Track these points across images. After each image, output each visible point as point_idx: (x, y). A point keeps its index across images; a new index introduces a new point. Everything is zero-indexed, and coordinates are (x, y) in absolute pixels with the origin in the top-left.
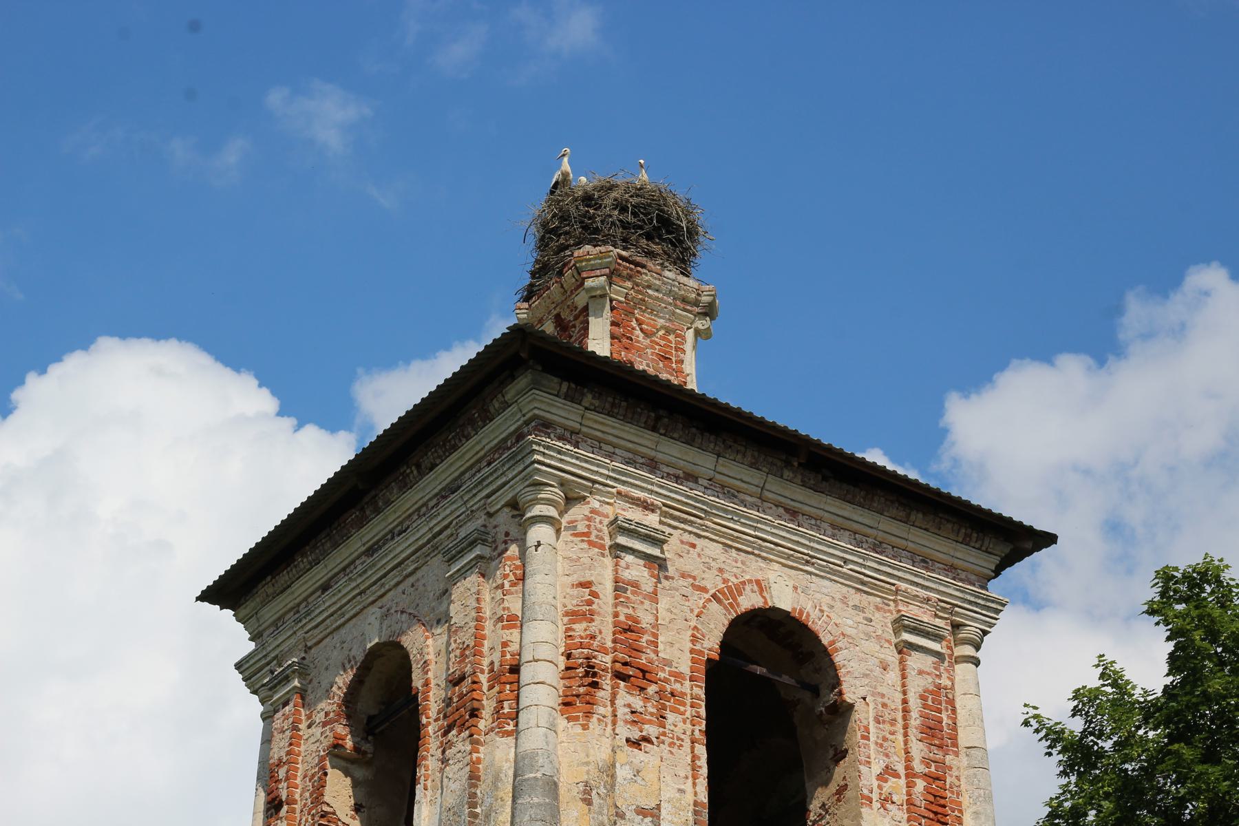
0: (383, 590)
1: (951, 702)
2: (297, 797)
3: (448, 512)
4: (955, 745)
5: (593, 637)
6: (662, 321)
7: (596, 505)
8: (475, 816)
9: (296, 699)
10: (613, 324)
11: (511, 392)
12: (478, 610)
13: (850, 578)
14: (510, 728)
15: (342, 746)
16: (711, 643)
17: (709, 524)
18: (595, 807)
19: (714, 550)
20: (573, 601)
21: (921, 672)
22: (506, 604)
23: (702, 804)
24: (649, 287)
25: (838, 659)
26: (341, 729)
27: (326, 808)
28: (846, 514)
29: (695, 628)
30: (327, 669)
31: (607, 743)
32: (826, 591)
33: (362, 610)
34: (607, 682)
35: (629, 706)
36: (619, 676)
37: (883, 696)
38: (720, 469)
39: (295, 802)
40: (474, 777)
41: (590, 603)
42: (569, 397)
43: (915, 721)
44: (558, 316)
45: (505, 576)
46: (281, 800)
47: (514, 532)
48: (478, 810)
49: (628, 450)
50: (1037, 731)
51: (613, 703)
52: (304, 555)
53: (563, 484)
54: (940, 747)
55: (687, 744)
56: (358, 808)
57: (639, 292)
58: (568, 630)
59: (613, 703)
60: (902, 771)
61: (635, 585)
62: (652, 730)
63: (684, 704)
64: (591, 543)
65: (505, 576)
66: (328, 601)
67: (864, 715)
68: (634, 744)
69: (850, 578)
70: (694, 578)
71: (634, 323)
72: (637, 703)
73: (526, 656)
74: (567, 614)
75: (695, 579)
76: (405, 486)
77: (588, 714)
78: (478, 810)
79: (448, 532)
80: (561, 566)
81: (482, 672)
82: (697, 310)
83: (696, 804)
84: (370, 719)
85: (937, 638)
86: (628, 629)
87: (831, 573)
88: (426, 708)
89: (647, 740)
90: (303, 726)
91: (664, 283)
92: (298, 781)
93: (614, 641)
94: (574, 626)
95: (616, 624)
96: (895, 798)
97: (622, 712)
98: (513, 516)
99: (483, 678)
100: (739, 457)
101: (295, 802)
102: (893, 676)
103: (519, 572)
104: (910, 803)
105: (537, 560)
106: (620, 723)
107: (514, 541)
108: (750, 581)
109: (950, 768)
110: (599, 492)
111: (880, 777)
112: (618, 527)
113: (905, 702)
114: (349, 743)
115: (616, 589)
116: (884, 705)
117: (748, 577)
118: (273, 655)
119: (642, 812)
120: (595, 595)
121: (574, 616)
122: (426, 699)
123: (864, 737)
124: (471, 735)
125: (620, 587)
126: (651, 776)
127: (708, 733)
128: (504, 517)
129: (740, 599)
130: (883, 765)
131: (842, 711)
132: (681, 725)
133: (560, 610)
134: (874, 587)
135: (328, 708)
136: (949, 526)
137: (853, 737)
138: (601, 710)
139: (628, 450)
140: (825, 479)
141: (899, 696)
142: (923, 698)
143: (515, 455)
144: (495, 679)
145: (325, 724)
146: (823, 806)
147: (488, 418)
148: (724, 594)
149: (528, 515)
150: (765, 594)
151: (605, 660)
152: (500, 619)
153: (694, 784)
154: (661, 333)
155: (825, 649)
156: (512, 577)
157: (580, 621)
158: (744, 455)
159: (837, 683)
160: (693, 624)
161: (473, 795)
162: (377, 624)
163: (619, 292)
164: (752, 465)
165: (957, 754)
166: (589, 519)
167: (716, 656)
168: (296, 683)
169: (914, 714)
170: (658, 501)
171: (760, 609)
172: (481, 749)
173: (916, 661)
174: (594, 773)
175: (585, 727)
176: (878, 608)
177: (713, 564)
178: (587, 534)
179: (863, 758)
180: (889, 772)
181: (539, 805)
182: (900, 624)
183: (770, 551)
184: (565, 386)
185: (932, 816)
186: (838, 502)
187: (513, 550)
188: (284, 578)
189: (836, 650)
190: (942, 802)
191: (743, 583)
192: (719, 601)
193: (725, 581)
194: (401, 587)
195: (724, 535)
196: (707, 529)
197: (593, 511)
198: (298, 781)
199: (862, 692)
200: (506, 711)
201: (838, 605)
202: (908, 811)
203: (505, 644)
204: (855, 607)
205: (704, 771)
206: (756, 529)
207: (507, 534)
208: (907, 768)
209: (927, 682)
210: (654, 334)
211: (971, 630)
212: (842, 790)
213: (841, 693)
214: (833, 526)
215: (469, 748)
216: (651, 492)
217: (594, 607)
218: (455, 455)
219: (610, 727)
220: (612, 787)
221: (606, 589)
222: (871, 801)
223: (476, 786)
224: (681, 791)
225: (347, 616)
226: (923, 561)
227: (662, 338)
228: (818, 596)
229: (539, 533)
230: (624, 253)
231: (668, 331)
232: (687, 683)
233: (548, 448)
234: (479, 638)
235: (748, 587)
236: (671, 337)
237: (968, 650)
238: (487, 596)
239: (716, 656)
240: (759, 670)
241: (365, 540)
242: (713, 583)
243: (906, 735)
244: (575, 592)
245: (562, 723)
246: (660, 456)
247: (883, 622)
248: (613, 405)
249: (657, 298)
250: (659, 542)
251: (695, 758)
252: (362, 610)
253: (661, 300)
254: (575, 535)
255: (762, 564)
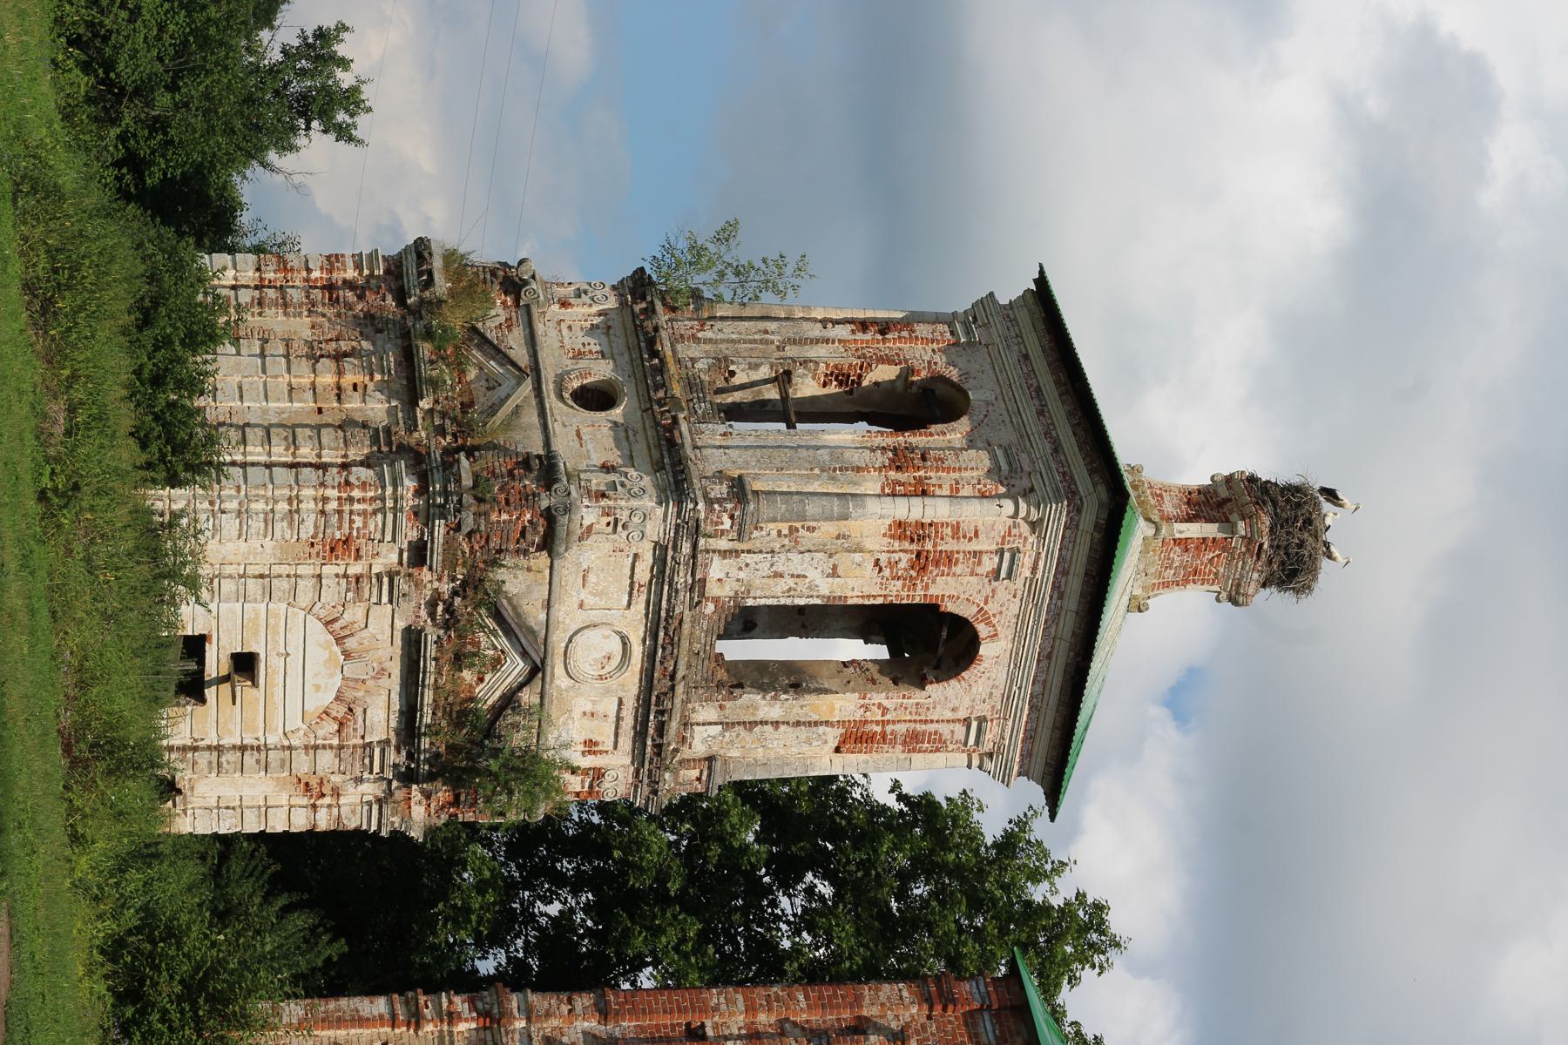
0: (1007, 399)
1: (937, 750)
2: (887, 345)
3: (1040, 446)
4: (909, 751)
5: (942, 539)
6: (1222, 570)
7: (1031, 540)
8: (835, 470)
9: (953, 340)
10: (1214, 539)
11: (1102, 489)
12: (966, 469)
13: (1010, 690)
14: (887, 491)
15: (913, 375)
16: (949, 607)
17: (1031, 606)
18: (836, 541)
19: (1014, 608)
20: (968, 528)
21: (952, 732)
22: (966, 487)
23: (846, 601)
24: (1244, 563)
25: (953, 682)
26: (924, 374)
27: (874, 366)
28: (1053, 689)
29: (958, 598)
30: (969, 361)
31: (877, 547)
32: (999, 675)
33: (1000, 385)
34: (914, 547)
35: (900, 560)
36: (918, 555)
37: (934, 708)
38: (1069, 613)
39: (884, 343)
40: (858, 469)
41: (964, 537)
42: (1097, 525)
43: (920, 727)
44: (1230, 500)
45: (985, 486)
46: (886, 334)
47: (1014, 490)
48: (838, 472)
49: (1071, 558)
50: (1025, 814)
51: (901, 551)
52: (1050, 342)
53: (1041, 520)
54: (905, 741)
55: (883, 593)
56: (876, 384)
57: (1239, 557)
58: (947, 524)
59: (901, 551)
60: (886, 718)
61: (979, 563)
62: (887, 572)
63: (909, 590)
64: (1004, 537)
65: (985, 486)
66: (1011, 358)
67: (918, 696)
68: (877, 563)
69: (1010, 690)
70: (993, 597)
71: (1217, 552)
72: (903, 565)
73: (927, 500)
74: (958, 523)
75: (993, 597)
76: (1070, 414)
77: (892, 537)
78: (838, 472)
79: (1028, 445)
80: (990, 520)
81: (926, 472)
82: (1233, 593)
83: (846, 597)
84: (933, 391)
85: (977, 743)
86: (950, 559)
87: (1011, 680)
88: (915, 435)
89: (881, 570)
90: (935, 346)
91: (1248, 573)
92: (898, 345)
93: (941, 551)
94: (950, 528)
95: (952, 552)
96: (868, 713)
97: (896, 556)
98: (1025, 490)
99: (922, 473)
100: (1077, 625)
101: (884, 343)
102: (949, 715)
103: (987, 494)
104: (866, 722)
105: (991, 506)
106: (888, 555)
107: (1008, 490)
108: (996, 630)
109: (893, 747)
110: (1039, 542)
111: (880, 705)
112: (1015, 553)
113: (932, 721)
114: (915, 378)
115: (975, 552)
116: (928, 709)
117: (999, 629)
118: (991, 320)
119: (835, 567)
120: (970, 539)
121: (956, 528)
122: (921, 435)
123: (904, 696)
124: (885, 467)
125: (976, 554)
126: (858, 572)
127: (891, 605)
128: (1026, 483)
129: (983, 624)
130: (889, 707)
131: (921, 683)
132: (895, 589)
133: (961, 520)
134: (1007, 706)
135: (939, 365)
136: (1055, 754)
137: (904, 690)
138: (897, 544)
139: (1071, 558)
140: (1073, 677)
141: (935, 718)
142: (936, 733)
143: (1058, 491)
144: (919, 481)
145: (929, 362)
146: (868, 670)
147: (1091, 472)
148: (984, 615)
149: (1020, 500)
150: (988, 639)
151: (929, 546)
152: (957, 483)
153: (858, 597)
154: (1214, 570)
155: (959, 674)
156: (984, 489)
157: (953, 531)
158: (1079, 628)
159: (938, 681)
160: (962, 596)
161: (847, 469)
162: (983, 398)
163: (1236, 542)
164: (1074, 632)
165: (903, 751)
166: (1020, 536)
167: (942, 609)
168: (963, 340)
169: (923, 727)
170: (1039, 576)
171: (978, 636)
172: (877, 473)
173: (960, 730)
174: (857, 541)
175: (884, 535)
176: (993, 707)
177: (1004, 608)
178: (1010, 535)
179: (890, 695)
180: (885, 711)
181: (832, 511)
182: (982, 720)
183: (1019, 642)
184: (1103, 522)
185: (859, 735)
186: (1059, 684)
187: (1002, 490)
188: (1041, 326)
189: (959, 681)
190: (869, 741)
191: (994, 626)
192: (979, 612)
193: (994, 615)
194: (1004, 412)
195: (1024, 615)
196: (1026, 606)
197: (1026, 539)
198: (898, 345)
199: (934, 695)
200: (897, 488)
201: (991, 683)
202: (860, 721)
203: (940, 486)
204: (991, 694)
205: (867, 602)
206: (1031, 634)
207: (1013, 486)
208: (888, 721)
209: (947, 736)
210: (1212, 565)
211: (989, 765)
212: (873, 682)
213: (931, 683)
214: (1045, 682)
215: (877, 466)
216: (1044, 572)
217: (962, 539)
218: (1077, 449)
219: (886, 549)
220: (849, 551)
221: (974, 546)
222: (864, 698)
223: (853, 470)
224: (853, 589)
225: (999, 374)
226: (1031, 737)
227: (1210, 571)
228: (995, 671)
229: (1009, 506)
230: (1265, 546)
231: (1216, 574)
232: (923, 593)
233: (1061, 513)
234: (948, 470)
235: (991, 629)
236: (1212, 576)
237: (976, 762)
238: (975, 474)
239: (942, 609)
240: (944, 634)
241: (1047, 386)
242: (991, 608)
243: (910, 721)
244: (972, 528)
245: (888, 522)
246: (1070, 577)
247: (983, 709)
248: (1096, 550)
249: (1237, 568)
250: (1009, 576)
251: (875, 597)
252: (1000, 385)
253: (1236, 570)
254: (1010, 527)
255: (1010, 637)
